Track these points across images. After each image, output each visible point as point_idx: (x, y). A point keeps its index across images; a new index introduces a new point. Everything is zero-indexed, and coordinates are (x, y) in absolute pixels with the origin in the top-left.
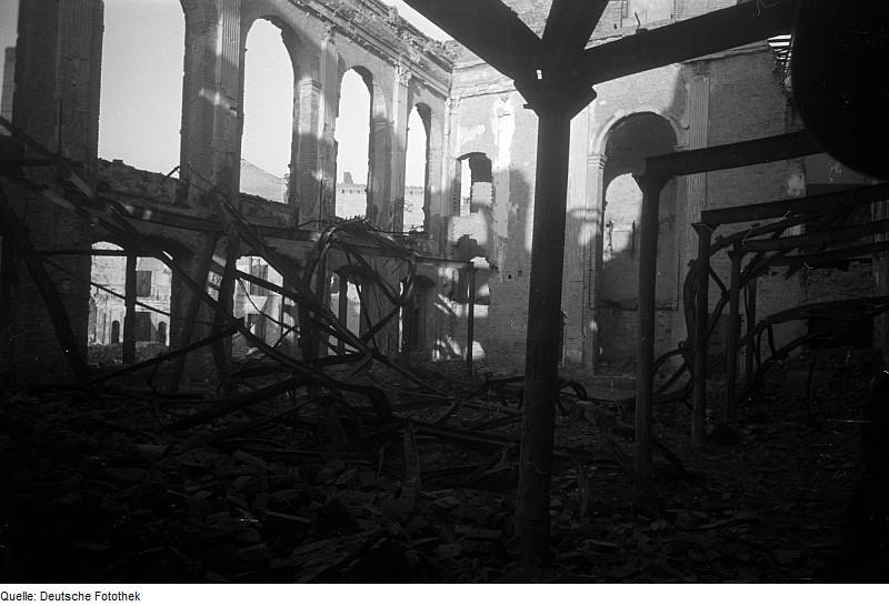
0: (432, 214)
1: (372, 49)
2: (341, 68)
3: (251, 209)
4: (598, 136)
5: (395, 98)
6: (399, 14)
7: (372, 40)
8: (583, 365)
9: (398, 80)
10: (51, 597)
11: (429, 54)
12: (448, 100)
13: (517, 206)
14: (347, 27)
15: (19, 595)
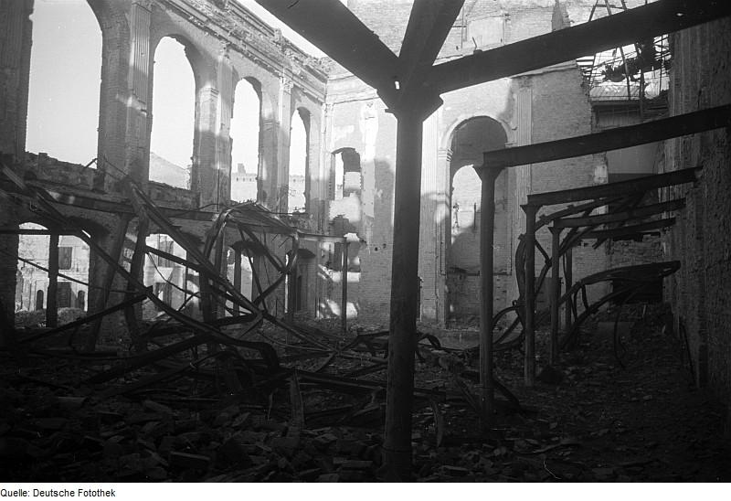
0: (311, 198)
1: (260, 63)
2: (235, 77)
3: (159, 194)
4: (445, 134)
5: (280, 103)
6: (283, 35)
8: (437, 321)
9: (282, 88)
10: (42, 493)
13: (381, 191)
14: (240, 44)
15: (16, 492)
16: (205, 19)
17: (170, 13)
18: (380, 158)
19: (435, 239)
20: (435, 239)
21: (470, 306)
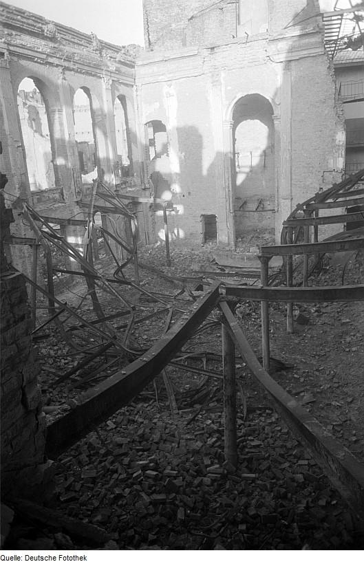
0: (134, 161)
1: (87, 73)
2: (72, 91)
4: (228, 108)
5: (105, 99)
6: (98, 38)
7: (86, 68)
9: (104, 87)
10: (31, 558)
11: (120, 62)
12: (135, 86)
13: (183, 154)
14: (71, 65)
15: (12, 557)
16: (44, 56)
17: (23, 62)
18: (182, 124)
19: (224, 188)
20: (224, 188)
21: (250, 224)
